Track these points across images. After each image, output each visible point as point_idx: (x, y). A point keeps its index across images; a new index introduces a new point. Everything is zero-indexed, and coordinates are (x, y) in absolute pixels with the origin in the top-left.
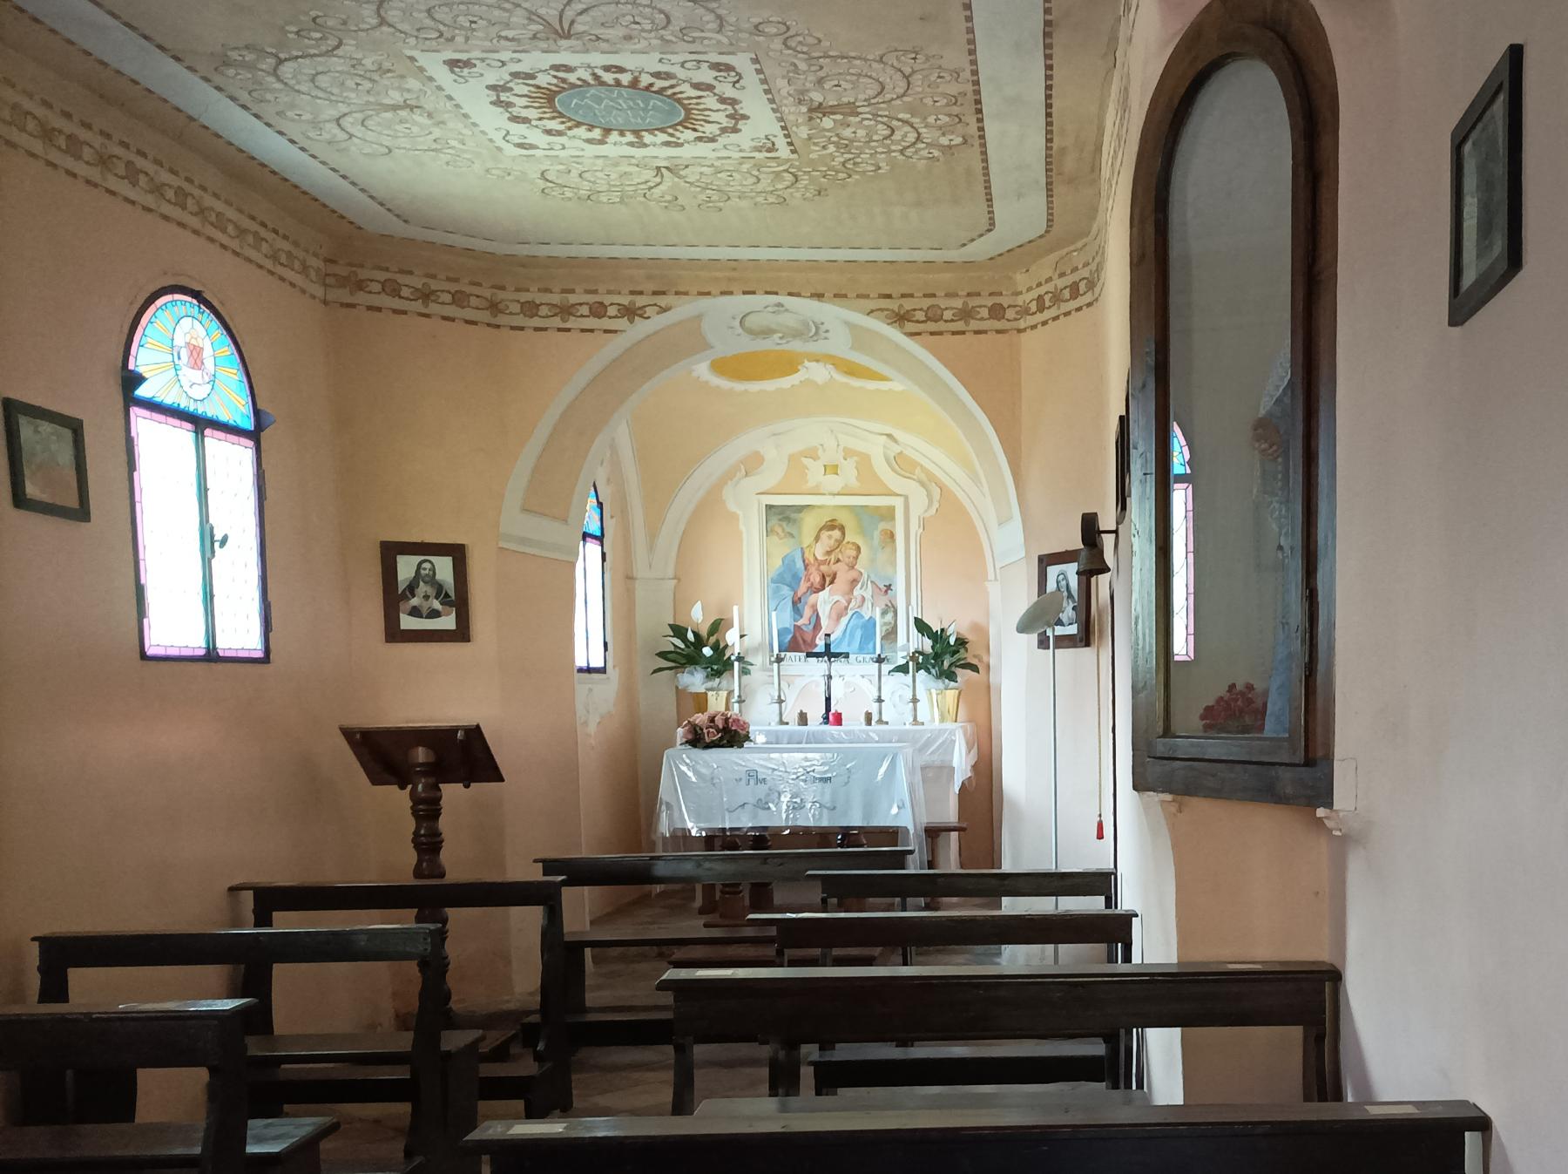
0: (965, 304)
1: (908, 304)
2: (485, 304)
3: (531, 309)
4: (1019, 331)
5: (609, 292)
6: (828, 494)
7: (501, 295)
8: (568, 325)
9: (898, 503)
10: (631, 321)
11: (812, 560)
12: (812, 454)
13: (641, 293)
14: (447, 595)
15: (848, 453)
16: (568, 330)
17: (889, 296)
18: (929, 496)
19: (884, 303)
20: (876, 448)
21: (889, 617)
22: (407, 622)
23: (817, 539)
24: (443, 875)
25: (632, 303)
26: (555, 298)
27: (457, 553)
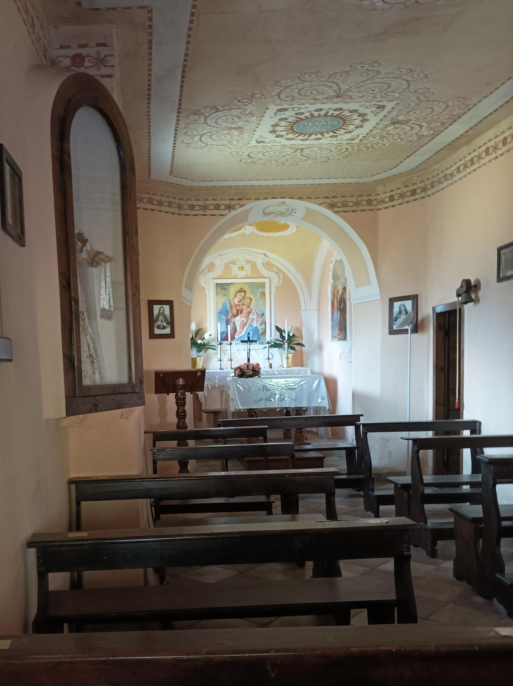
0: (357, 199)
1: (335, 200)
2: (177, 206)
3: (192, 207)
4: (378, 209)
5: (221, 200)
6: (239, 278)
7: (182, 202)
8: (205, 213)
9: (267, 281)
10: (230, 211)
11: (233, 304)
12: (234, 263)
13: (233, 200)
14: (168, 320)
15: (248, 262)
16: (206, 215)
17: (327, 197)
18: (279, 278)
19: (326, 200)
20: (259, 260)
21: (263, 326)
22: (157, 331)
23: (235, 296)
24: (187, 428)
25: (230, 204)
26: (201, 203)
27: (170, 303)
